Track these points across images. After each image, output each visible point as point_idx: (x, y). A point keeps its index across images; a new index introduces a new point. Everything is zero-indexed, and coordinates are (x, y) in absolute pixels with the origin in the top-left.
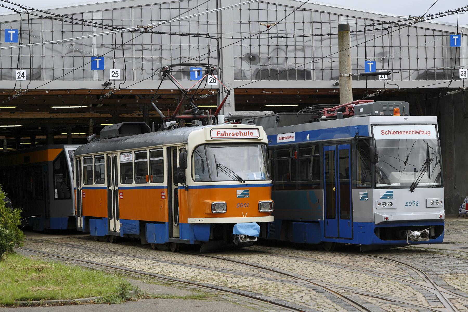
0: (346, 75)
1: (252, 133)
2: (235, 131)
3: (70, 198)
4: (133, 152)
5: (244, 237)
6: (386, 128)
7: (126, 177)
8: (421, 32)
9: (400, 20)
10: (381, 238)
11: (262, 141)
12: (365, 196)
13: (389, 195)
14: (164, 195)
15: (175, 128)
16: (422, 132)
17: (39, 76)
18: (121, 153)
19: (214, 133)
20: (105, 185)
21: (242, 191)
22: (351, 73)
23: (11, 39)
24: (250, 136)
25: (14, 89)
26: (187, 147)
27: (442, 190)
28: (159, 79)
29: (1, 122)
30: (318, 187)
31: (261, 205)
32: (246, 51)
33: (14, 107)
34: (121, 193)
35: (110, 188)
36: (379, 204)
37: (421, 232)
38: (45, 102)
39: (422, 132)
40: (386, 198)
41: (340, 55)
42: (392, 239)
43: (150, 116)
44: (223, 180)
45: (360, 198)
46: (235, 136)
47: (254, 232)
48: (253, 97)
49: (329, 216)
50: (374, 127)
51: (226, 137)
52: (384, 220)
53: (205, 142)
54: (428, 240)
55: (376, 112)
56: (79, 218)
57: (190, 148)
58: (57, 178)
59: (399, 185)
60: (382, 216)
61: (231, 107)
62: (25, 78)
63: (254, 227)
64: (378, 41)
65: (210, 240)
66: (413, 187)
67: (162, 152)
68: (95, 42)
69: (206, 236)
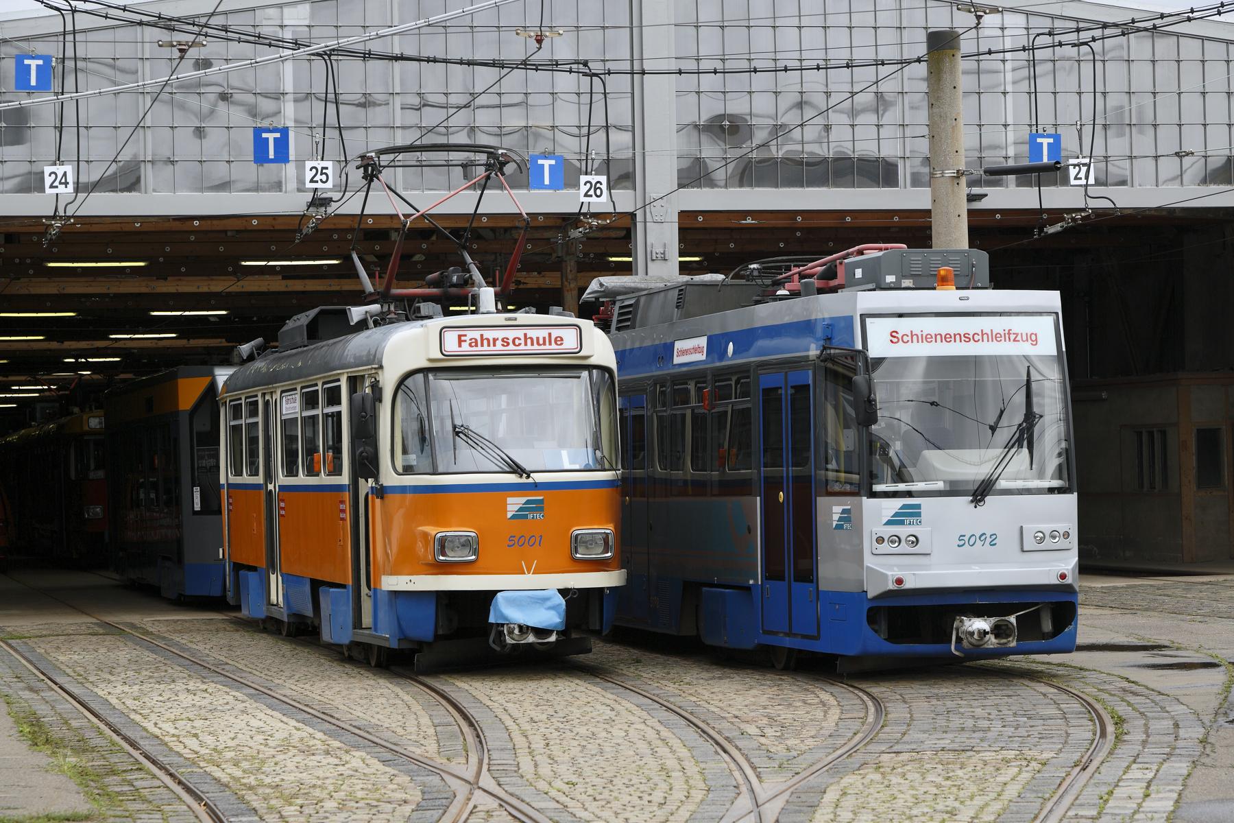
0: (949, 173)
2: (511, 334)
3: (220, 512)
5: (516, 631)
6: (910, 326)
8: (1190, 49)
9: (1137, 16)
10: (893, 637)
12: (847, 516)
13: (912, 514)
14: (343, 511)
15: (376, 324)
16: (1012, 337)
17: (133, 180)
18: (282, 392)
21: (524, 500)
22: (963, 168)
23: (33, 83)
24: (554, 348)
25: (579, 213)
26: (380, 378)
27: (1071, 500)
29: (48, 304)
30: (742, 488)
31: (577, 541)
32: (711, 108)
33: (697, 259)
36: (880, 540)
37: (993, 620)
38: (222, 249)
39: (1012, 337)
40: (902, 523)
41: (931, 116)
42: (918, 640)
44: (471, 469)
45: (834, 524)
46: (511, 347)
47: (550, 616)
48: (798, 234)
49: (773, 573)
50: (868, 321)
51: (486, 349)
52: (891, 586)
53: (425, 364)
54: (1013, 644)
55: (890, 279)
58: (201, 458)
59: (940, 485)
60: (885, 576)
61: (669, 263)
62: (71, 188)
63: (549, 604)
64: (1067, 82)
66: (981, 491)
68: (289, 87)
69: (424, 626)
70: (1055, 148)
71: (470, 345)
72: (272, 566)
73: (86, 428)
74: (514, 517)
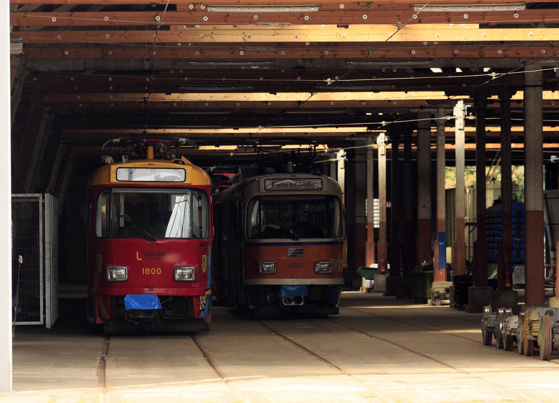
21: (295, 249)
73: (113, 180)
74: (291, 256)
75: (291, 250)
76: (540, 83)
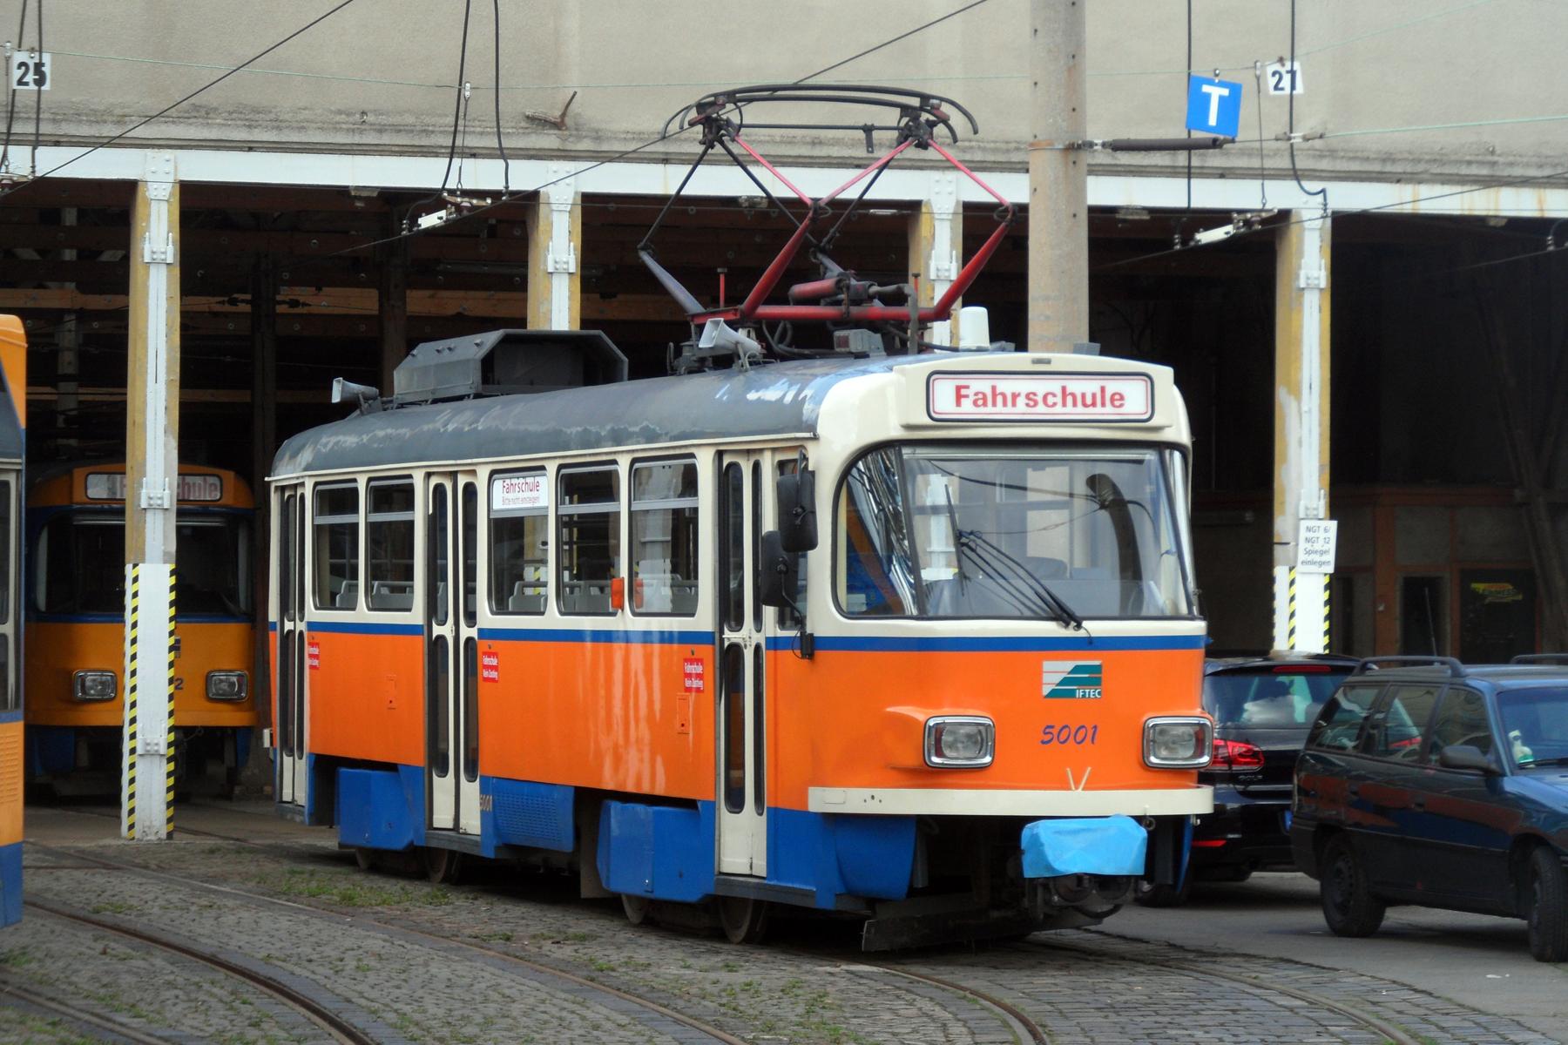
1: (1118, 399)
2: (1041, 386)
4: (552, 468)
7: (508, 585)
11: (1168, 435)
19: (944, 392)
20: (416, 616)
21: (1069, 665)
24: (1108, 412)
28: (702, 143)
31: (1149, 739)
34: (490, 655)
35: (437, 630)
43: (281, 309)
46: (1041, 408)
47: (1123, 855)
48: (758, 239)
51: (999, 411)
56: (288, 761)
57: (827, 460)
65: (912, 892)
67: (409, 490)
69: (896, 871)
70: (1230, 106)
71: (975, 403)
72: (438, 762)
74: (1053, 694)
75: (1055, 670)
76: (864, 608)
